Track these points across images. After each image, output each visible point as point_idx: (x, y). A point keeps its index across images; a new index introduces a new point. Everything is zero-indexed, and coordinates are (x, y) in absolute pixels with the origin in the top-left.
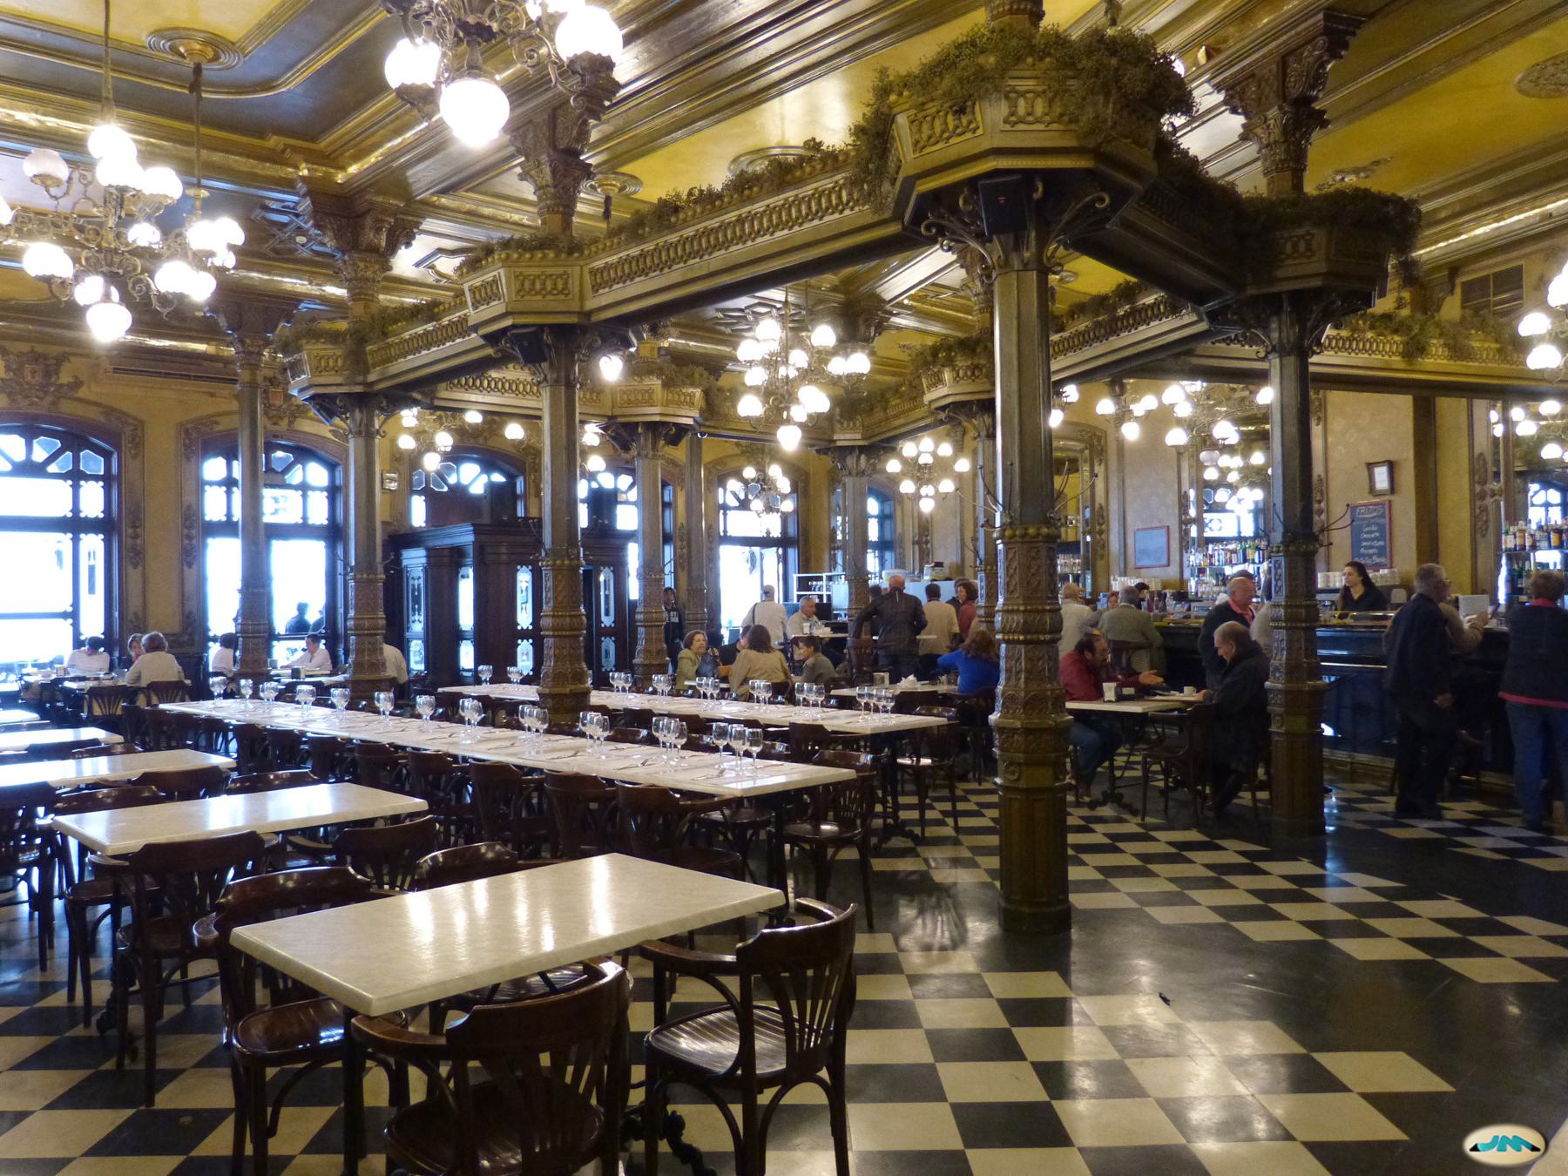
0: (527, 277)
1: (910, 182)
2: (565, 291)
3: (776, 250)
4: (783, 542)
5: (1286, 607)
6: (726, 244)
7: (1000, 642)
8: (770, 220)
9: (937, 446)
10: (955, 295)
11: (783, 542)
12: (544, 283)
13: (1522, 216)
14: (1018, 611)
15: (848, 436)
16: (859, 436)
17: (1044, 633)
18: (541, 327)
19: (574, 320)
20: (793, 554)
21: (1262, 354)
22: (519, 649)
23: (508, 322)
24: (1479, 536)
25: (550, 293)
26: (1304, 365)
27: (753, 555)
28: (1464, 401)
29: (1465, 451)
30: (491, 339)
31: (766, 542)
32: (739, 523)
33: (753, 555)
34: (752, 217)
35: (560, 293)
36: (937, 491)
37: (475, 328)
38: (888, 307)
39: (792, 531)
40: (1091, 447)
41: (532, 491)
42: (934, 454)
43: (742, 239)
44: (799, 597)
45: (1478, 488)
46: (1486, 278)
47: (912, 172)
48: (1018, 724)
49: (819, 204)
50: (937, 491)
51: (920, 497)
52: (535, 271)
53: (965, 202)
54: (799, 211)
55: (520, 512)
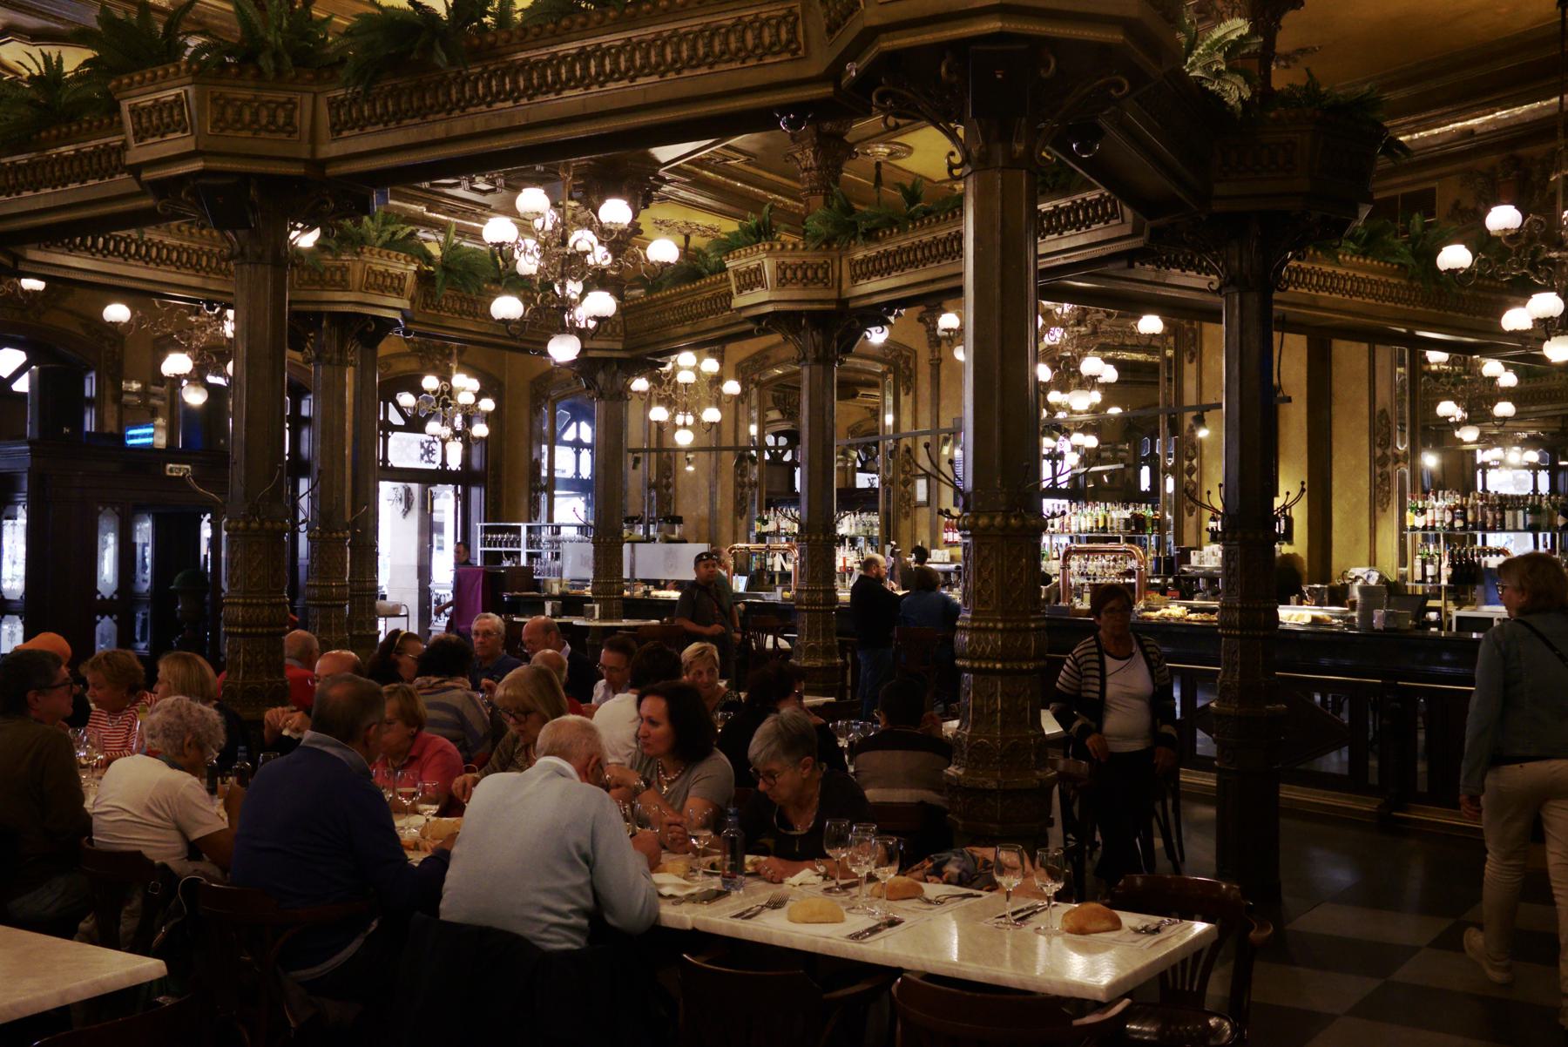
0: (229, 102)
1: (870, 35)
2: (290, 127)
3: (640, 101)
4: (462, 479)
5: (1241, 610)
6: (558, 86)
7: (964, 669)
8: (631, 60)
9: (699, 361)
10: (747, 163)
11: (462, 479)
12: (256, 113)
13: (896, 42)
14: (994, 629)
15: (603, 345)
16: (619, 346)
17: (1027, 659)
18: (246, 177)
19: (297, 170)
20: (476, 494)
21: (1215, 287)
22: (99, 628)
23: (197, 165)
24: (1378, 509)
25: (265, 128)
26: (1267, 303)
27: (408, 491)
28: (1365, 346)
29: (1365, 408)
30: (161, 188)
31: (442, 476)
32: (403, 450)
33: (408, 491)
34: (602, 53)
35: (280, 130)
36: (698, 420)
37: (135, 170)
38: (661, 172)
39: (476, 462)
40: (896, 371)
41: (109, 393)
42: (696, 370)
43: (584, 82)
44: (486, 554)
45: (1379, 452)
46: (1394, 199)
47: (875, 21)
48: (993, 785)
49: (710, 44)
50: (698, 420)
51: (676, 428)
52: (246, 94)
53: (949, 71)
54: (678, 52)
55: (90, 423)
